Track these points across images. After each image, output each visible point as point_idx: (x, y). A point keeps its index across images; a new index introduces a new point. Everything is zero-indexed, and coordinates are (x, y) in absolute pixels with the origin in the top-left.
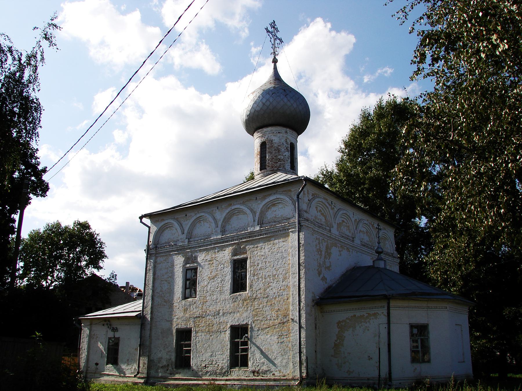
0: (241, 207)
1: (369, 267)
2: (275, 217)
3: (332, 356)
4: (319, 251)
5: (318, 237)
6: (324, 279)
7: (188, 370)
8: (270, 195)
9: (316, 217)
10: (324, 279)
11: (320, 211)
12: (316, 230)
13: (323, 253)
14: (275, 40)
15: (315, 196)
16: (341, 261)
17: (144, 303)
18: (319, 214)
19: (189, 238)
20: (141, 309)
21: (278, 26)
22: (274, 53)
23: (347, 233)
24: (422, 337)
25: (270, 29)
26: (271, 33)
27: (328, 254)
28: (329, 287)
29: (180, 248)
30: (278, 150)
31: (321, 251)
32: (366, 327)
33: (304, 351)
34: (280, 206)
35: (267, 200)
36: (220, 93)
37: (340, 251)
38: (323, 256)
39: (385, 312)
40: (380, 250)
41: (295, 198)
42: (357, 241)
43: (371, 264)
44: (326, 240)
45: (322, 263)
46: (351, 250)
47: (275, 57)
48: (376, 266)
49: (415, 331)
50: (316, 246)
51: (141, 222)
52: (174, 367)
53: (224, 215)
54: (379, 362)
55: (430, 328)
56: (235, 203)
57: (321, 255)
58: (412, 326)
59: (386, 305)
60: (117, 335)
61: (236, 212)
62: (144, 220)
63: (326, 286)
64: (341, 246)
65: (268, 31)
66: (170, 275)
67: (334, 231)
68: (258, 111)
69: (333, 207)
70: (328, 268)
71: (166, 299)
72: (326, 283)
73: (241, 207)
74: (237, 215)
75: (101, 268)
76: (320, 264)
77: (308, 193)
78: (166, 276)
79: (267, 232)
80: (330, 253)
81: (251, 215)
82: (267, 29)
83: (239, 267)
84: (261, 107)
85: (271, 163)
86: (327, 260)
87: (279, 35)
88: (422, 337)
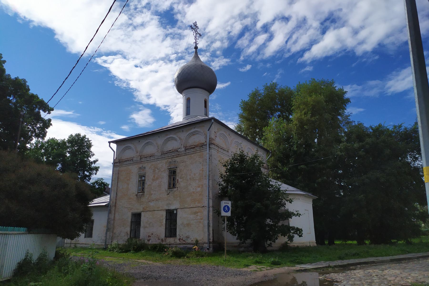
8: (191, 129)
14: (196, 34)
17: (110, 197)
20: (108, 201)
26: (194, 29)
33: (211, 225)
36: (17, 79)
47: (196, 45)
51: (110, 146)
62: (112, 144)
75: (163, 40)
83: (173, 173)
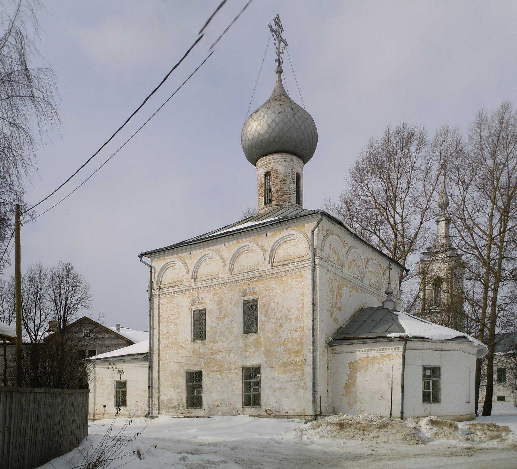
0: (250, 244)
1: (378, 309)
2: (288, 256)
3: (343, 395)
4: (332, 291)
5: (331, 277)
6: (336, 320)
7: (199, 410)
9: (329, 255)
10: (336, 320)
11: (333, 248)
12: (330, 269)
13: (335, 293)
14: (279, 42)
15: (329, 233)
16: (352, 302)
18: (332, 252)
19: (195, 278)
21: (282, 23)
22: (279, 60)
23: (358, 273)
24: (434, 379)
25: (274, 27)
27: (340, 295)
28: (340, 328)
29: (186, 288)
30: (284, 182)
31: (333, 292)
32: (379, 368)
34: (293, 243)
35: (279, 237)
37: (350, 292)
38: (335, 296)
39: (401, 354)
40: (390, 291)
41: (310, 234)
42: (366, 282)
43: (380, 305)
44: (338, 280)
45: (334, 304)
46: (360, 291)
48: (385, 307)
49: (428, 373)
50: (329, 285)
52: (185, 407)
53: (233, 252)
54: (391, 402)
55: (443, 370)
56: (244, 240)
57: (333, 295)
58: (425, 368)
59: (401, 348)
60: (124, 378)
61: (245, 249)
63: (337, 327)
64: (352, 286)
65: (272, 30)
66: (177, 316)
67: (345, 270)
68: (262, 135)
69: (345, 244)
70: (339, 309)
71: (173, 341)
72: (337, 324)
73: (250, 244)
74: (246, 253)
76: (332, 304)
77: (322, 229)
78: (172, 318)
79: (279, 271)
80: (342, 293)
81: (261, 253)
82: (270, 26)
84: (266, 129)
85: (276, 196)
86: (339, 301)
87: (284, 35)
88: (434, 379)
